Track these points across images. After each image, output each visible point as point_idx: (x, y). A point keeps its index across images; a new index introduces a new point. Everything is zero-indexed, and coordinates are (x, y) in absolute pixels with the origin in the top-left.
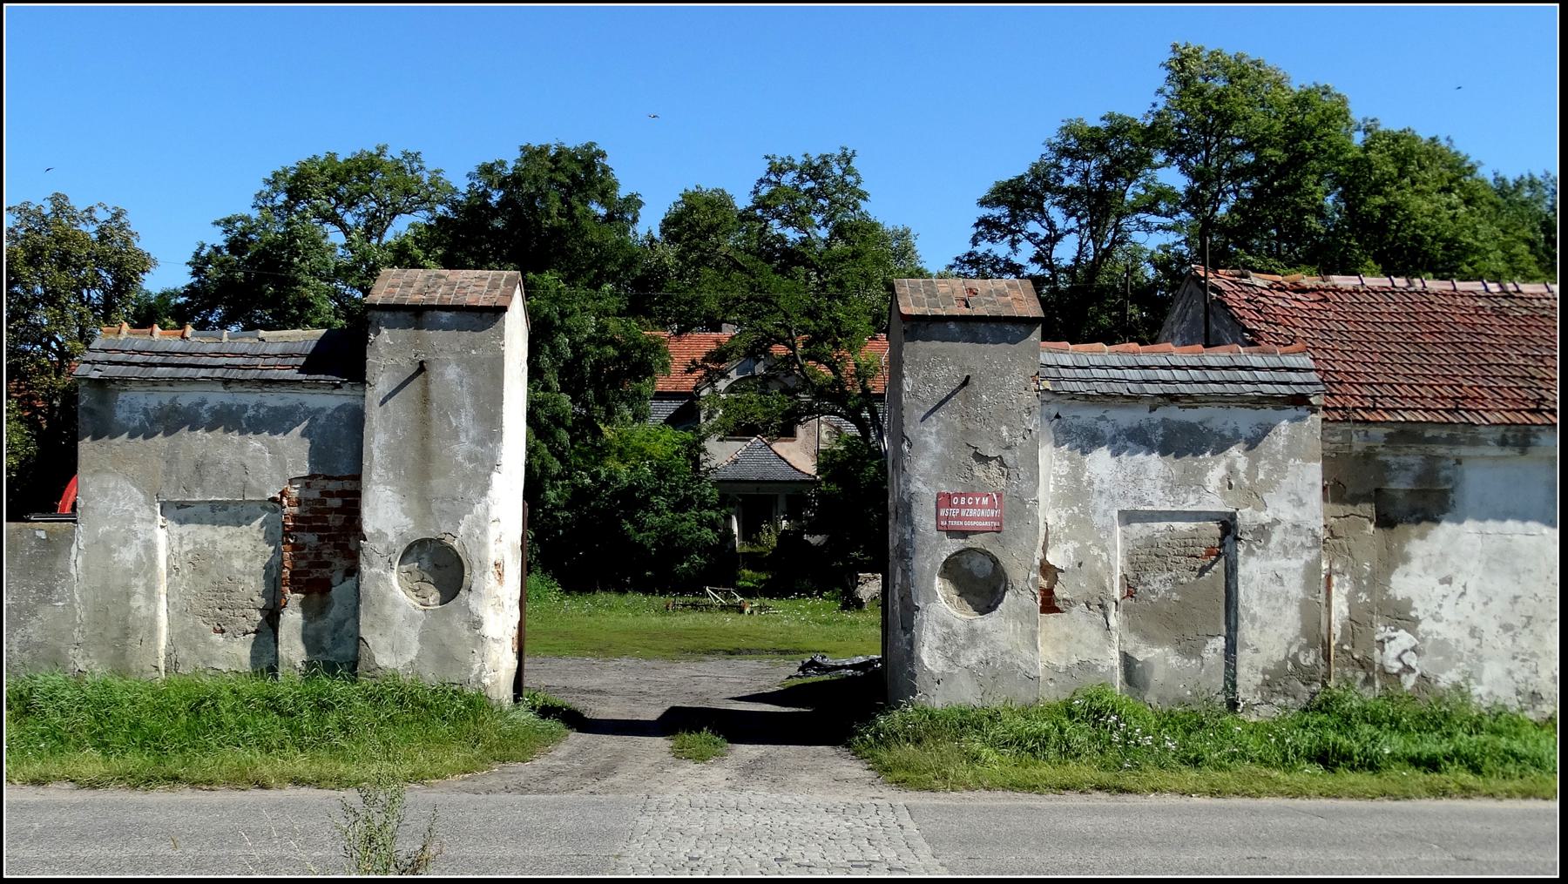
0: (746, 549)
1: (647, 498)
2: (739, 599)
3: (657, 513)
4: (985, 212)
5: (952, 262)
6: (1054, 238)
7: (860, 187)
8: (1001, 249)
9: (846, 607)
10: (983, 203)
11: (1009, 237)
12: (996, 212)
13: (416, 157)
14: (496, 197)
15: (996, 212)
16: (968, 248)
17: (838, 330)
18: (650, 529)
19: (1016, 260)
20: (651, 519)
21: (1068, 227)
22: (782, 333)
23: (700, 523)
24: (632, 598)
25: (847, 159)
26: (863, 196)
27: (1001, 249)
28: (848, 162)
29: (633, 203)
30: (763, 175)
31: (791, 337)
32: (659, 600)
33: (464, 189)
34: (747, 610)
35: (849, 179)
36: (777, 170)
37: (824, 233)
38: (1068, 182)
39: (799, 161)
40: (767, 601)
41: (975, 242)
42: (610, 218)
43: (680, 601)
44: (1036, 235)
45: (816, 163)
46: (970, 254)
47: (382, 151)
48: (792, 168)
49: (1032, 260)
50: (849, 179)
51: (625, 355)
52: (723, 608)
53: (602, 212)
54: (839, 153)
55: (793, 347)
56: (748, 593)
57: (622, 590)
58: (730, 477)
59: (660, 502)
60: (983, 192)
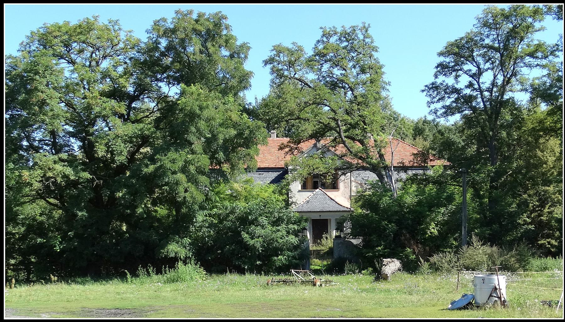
0: (315, 248)
1: (256, 219)
2: (313, 277)
3: (263, 227)
4: (442, 59)
5: (423, 88)
6: (480, 73)
7: (375, 44)
8: (450, 81)
9: (377, 279)
10: (441, 54)
11: (454, 74)
12: (448, 60)
13: (116, 22)
14: (164, 43)
15: (448, 60)
16: (432, 80)
17: (364, 122)
18: (258, 237)
19: (458, 86)
20: (259, 231)
21: (486, 68)
22: (333, 124)
23: (288, 233)
24: (249, 277)
25: (366, 29)
26: (375, 49)
27: (450, 81)
28: (366, 31)
29: (245, 48)
30: (319, 38)
31: (339, 126)
32: (263, 279)
33: (146, 40)
34: (318, 283)
35: (367, 40)
36: (327, 35)
37: (355, 71)
38: (487, 41)
39: (339, 30)
40: (329, 277)
41: (436, 76)
42: (232, 56)
43: (278, 278)
44: (470, 70)
45: (348, 31)
46: (433, 84)
47: (96, 18)
48: (336, 33)
49: (467, 87)
50: (367, 40)
51: (240, 135)
52: (303, 282)
53: (227, 53)
54: (361, 25)
55: (339, 133)
56: (317, 272)
57: (242, 272)
58: (305, 210)
59: (263, 220)
60: (441, 48)
